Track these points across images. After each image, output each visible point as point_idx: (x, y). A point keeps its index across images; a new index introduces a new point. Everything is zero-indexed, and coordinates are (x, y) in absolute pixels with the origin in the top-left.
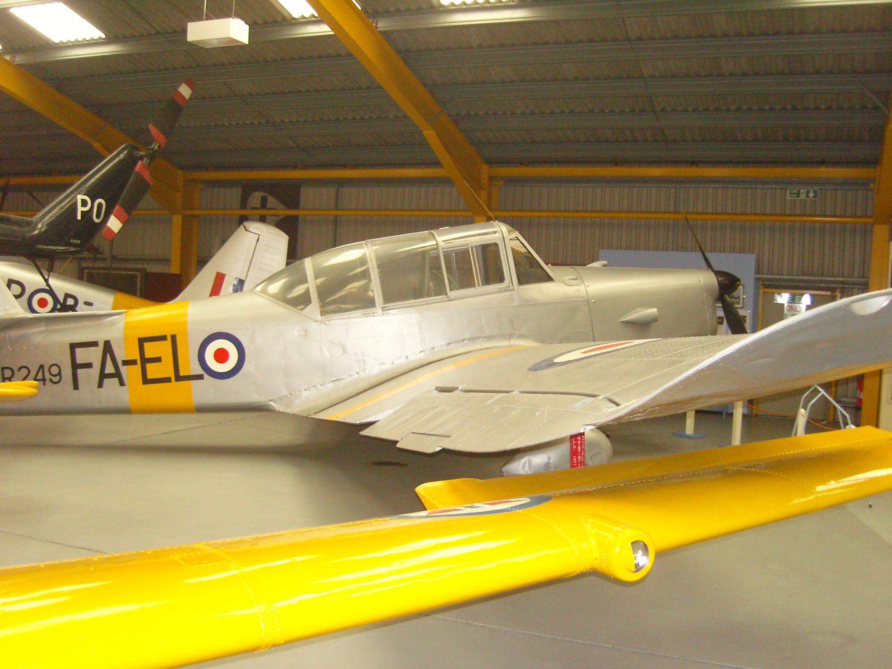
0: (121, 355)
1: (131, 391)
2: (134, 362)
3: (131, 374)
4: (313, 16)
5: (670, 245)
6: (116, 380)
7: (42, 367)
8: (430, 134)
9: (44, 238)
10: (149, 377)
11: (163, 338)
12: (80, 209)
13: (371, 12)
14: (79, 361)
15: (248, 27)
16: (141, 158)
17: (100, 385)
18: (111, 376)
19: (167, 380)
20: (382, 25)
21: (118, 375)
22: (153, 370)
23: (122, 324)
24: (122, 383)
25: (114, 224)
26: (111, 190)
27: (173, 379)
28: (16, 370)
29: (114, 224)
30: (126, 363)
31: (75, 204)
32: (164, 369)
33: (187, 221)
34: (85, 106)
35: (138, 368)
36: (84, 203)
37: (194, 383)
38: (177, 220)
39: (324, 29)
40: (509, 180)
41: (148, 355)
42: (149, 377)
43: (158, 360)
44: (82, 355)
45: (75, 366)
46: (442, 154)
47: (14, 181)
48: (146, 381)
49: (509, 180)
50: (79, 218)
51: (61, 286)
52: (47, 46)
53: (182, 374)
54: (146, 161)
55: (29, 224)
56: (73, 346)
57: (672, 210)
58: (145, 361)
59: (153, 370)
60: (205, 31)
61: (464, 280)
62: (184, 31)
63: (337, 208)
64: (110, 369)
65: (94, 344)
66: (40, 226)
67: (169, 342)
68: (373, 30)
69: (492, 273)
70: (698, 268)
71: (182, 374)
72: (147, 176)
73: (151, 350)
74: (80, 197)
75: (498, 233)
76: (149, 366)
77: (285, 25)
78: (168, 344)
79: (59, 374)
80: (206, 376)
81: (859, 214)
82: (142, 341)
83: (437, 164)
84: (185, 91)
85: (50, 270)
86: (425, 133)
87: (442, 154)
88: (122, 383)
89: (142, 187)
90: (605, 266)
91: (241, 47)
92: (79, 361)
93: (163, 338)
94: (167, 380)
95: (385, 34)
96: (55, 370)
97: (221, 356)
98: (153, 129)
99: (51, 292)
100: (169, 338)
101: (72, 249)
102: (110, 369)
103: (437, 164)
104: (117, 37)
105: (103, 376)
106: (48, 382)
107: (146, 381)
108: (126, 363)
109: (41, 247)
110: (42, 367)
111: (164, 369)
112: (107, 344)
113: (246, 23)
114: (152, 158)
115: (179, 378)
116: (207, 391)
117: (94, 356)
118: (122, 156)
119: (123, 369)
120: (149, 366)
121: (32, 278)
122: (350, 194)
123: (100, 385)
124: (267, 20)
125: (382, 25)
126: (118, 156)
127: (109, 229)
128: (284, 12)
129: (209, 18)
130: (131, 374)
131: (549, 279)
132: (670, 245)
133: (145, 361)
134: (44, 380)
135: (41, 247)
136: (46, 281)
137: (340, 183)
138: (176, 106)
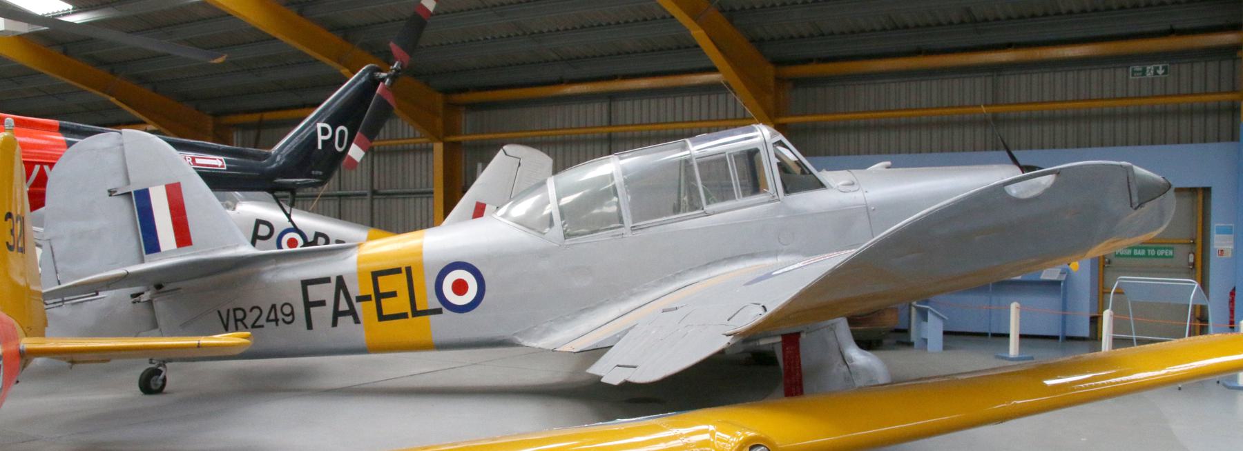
0: (354, 290)
1: (368, 327)
2: (366, 298)
3: (366, 310)
7: (274, 306)
8: (698, 34)
9: (284, 171)
12: (321, 138)
14: (311, 299)
17: (335, 324)
18: (344, 313)
19: (404, 316)
21: (352, 312)
22: (389, 306)
24: (357, 321)
25: (356, 152)
27: (410, 315)
28: (247, 310)
29: (356, 152)
30: (360, 299)
31: (315, 133)
32: (400, 304)
33: (452, 151)
34: (331, 30)
35: (372, 304)
36: (325, 132)
37: (432, 317)
38: (438, 147)
40: (799, 82)
41: (382, 290)
43: (393, 294)
44: (315, 293)
45: (308, 305)
47: (268, 116)
48: (382, 317)
49: (799, 82)
50: (320, 147)
51: (308, 222)
53: (419, 308)
55: (267, 156)
56: (306, 283)
58: (380, 296)
59: (389, 306)
61: (722, 192)
63: (610, 124)
64: (343, 306)
65: (326, 280)
66: (278, 158)
69: (754, 184)
70: (1000, 162)
73: (385, 284)
74: (320, 125)
75: (762, 135)
76: (384, 302)
79: (292, 313)
81: (1196, 90)
82: (376, 275)
83: (713, 70)
85: (292, 205)
88: (357, 321)
89: (385, 112)
90: (888, 167)
92: (311, 299)
93: (397, 271)
94: (404, 316)
96: (287, 310)
97: (460, 287)
98: (393, 46)
99: (295, 229)
100: (404, 270)
101: (313, 181)
102: (343, 306)
105: (337, 314)
106: (280, 322)
107: (382, 317)
108: (360, 299)
110: (274, 306)
111: (400, 304)
112: (340, 279)
115: (416, 313)
116: (444, 326)
117: (326, 293)
118: (363, 79)
119: (358, 306)
120: (384, 302)
121: (275, 215)
122: (625, 109)
123: (335, 324)
126: (354, 80)
127: (351, 159)
130: (366, 310)
131: (820, 185)
133: (380, 296)
134: (276, 320)
136: (289, 216)
137: (612, 97)
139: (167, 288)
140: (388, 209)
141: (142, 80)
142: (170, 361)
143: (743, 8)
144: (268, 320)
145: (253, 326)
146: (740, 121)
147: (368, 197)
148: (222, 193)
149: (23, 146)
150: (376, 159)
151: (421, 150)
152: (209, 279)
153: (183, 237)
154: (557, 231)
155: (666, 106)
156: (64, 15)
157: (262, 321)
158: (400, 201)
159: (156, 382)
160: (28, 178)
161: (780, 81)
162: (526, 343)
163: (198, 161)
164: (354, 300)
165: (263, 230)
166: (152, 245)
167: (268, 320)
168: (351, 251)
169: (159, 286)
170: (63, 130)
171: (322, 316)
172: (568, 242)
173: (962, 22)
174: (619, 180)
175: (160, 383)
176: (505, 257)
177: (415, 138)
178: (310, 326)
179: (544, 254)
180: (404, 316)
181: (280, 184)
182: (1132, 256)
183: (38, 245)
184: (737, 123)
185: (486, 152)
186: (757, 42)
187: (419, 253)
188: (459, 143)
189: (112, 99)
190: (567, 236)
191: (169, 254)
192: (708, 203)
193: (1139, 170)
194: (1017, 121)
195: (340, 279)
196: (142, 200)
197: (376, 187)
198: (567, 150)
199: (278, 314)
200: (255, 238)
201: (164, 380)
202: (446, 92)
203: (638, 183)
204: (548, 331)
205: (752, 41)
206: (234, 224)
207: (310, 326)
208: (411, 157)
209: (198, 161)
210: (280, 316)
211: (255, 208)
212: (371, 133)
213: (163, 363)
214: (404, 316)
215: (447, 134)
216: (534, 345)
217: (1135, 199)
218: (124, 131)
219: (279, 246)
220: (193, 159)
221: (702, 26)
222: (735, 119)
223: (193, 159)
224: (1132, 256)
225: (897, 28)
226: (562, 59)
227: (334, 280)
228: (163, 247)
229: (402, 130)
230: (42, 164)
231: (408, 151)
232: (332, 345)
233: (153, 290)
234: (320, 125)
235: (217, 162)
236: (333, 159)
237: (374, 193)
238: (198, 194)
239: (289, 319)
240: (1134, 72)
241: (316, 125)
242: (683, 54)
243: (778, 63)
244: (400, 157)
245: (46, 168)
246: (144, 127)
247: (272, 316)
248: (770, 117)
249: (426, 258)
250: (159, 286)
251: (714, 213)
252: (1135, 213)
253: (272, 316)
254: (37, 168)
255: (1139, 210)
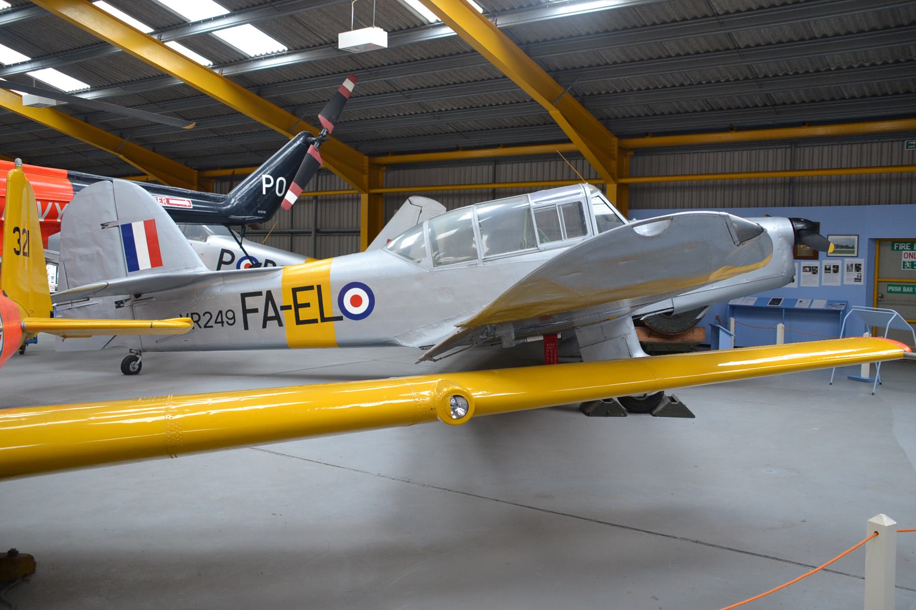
0: (279, 302)
1: (290, 330)
2: (289, 307)
3: (288, 316)
4: (438, 21)
5: (786, 201)
6: (276, 322)
7: (221, 312)
8: (555, 114)
9: (236, 210)
10: (301, 319)
11: (311, 288)
12: (265, 186)
13: (492, 12)
14: (248, 308)
15: (386, 33)
16: (313, 143)
17: (264, 326)
18: (272, 318)
19: (315, 321)
20: (501, 22)
21: (277, 318)
22: (304, 314)
23: (280, 278)
24: (281, 324)
25: (291, 197)
26: (288, 170)
27: (319, 320)
30: (283, 308)
35: (292, 311)
36: (268, 181)
38: (365, 197)
39: (447, 32)
42: (301, 319)
44: (251, 303)
45: (246, 311)
46: (568, 130)
48: (299, 322)
50: (264, 193)
51: (260, 252)
52: (244, 59)
53: (326, 316)
54: (317, 144)
56: (244, 296)
57: (788, 168)
58: (297, 306)
59: (304, 314)
60: (350, 40)
62: (336, 42)
63: (494, 182)
64: (271, 313)
65: (259, 294)
66: (233, 201)
67: (315, 291)
68: (492, 27)
71: (326, 316)
72: (317, 156)
73: (302, 297)
74: (264, 177)
77: (425, 29)
78: (315, 292)
79: (234, 317)
80: (344, 317)
82: (295, 291)
83: (569, 141)
84: (349, 85)
85: (243, 236)
86: (551, 113)
87: (568, 130)
88: (281, 324)
91: (380, 51)
92: (248, 308)
93: (311, 288)
94: (315, 321)
95: (506, 31)
96: (230, 315)
97: (356, 301)
99: (248, 257)
100: (315, 288)
102: (271, 313)
103: (569, 141)
104: (296, 49)
105: (266, 319)
106: (225, 324)
107: (299, 322)
108: (283, 308)
109: (233, 217)
110: (221, 312)
112: (269, 293)
113: (385, 30)
114: (321, 141)
115: (324, 319)
116: (346, 330)
117: (258, 303)
118: (298, 142)
119: (282, 314)
121: (231, 244)
122: (505, 170)
123: (264, 326)
124: (402, 25)
125: (501, 22)
127: (287, 201)
128: (421, 18)
129: (356, 28)
130: (288, 316)
132: (786, 201)
133: (297, 306)
135: (233, 217)
136: (240, 244)
137: (496, 160)
138: (343, 100)
139: (144, 296)
140: (321, 241)
141: (143, 142)
142: (145, 351)
143: (592, 94)
144: (216, 322)
145: (205, 326)
146: (571, 180)
147: (313, 234)
148: (189, 226)
149: (36, 188)
150: (319, 205)
151: (353, 199)
152: (175, 290)
153: (156, 260)
154: (428, 261)
155: (538, 167)
156: (80, 93)
157: (212, 323)
158: (337, 238)
159: (134, 366)
160: (43, 213)
161: (623, 150)
162: (404, 344)
163: (171, 202)
164: (279, 309)
165: (227, 257)
166: (133, 265)
167: (216, 322)
168: (279, 272)
169: (138, 296)
170: (70, 177)
171: (255, 320)
172: (436, 269)
173: (765, 105)
174: (475, 224)
175: (137, 367)
176: (390, 279)
177: (348, 190)
178: (246, 328)
179: (419, 277)
180: (315, 321)
181: (234, 219)
182: (902, 292)
183: (48, 261)
184: (565, 183)
185: (399, 200)
186: (606, 121)
187: (327, 274)
188: (381, 194)
189: (121, 156)
190: (437, 263)
191: (146, 271)
192: (542, 242)
193: (734, 217)
194: (810, 183)
195: (269, 293)
196: (127, 231)
197: (318, 227)
198: (453, 199)
199: (223, 318)
200: (221, 262)
201: (140, 364)
202: (371, 155)
203: (488, 225)
204: (419, 335)
205: (601, 119)
206: (197, 252)
207: (246, 328)
208: (346, 204)
209: (171, 202)
210: (225, 319)
211: (219, 241)
212: (302, 184)
213: (140, 352)
214: (315, 321)
215: (370, 187)
216: (410, 345)
217: (736, 238)
218: (115, 180)
219: (238, 267)
220: (168, 200)
221: (557, 107)
222: (563, 180)
223: (168, 200)
224: (902, 292)
225: (713, 110)
226: (458, 132)
227: (264, 294)
228: (141, 267)
229: (341, 185)
230: (54, 201)
231: (335, 200)
232: (262, 342)
233: (133, 297)
234: (264, 177)
235: (185, 203)
236: (274, 201)
237: (317, 231)
238: (169, 228)
239: (231, 322)
240: (908, 145)
241: (264, 177)
242: (545, 130)
243: (621, 136)
244: (337, 204)
245: (57, 204)
246: (145, 178)
247: (220, 320)
248: (613, 178)
249: (332, 278)
250: (138, 296)
251: (545, 250)
252: (739, 248)
253: (220, 320)
254: (50, 204)
255: (741, 246)
